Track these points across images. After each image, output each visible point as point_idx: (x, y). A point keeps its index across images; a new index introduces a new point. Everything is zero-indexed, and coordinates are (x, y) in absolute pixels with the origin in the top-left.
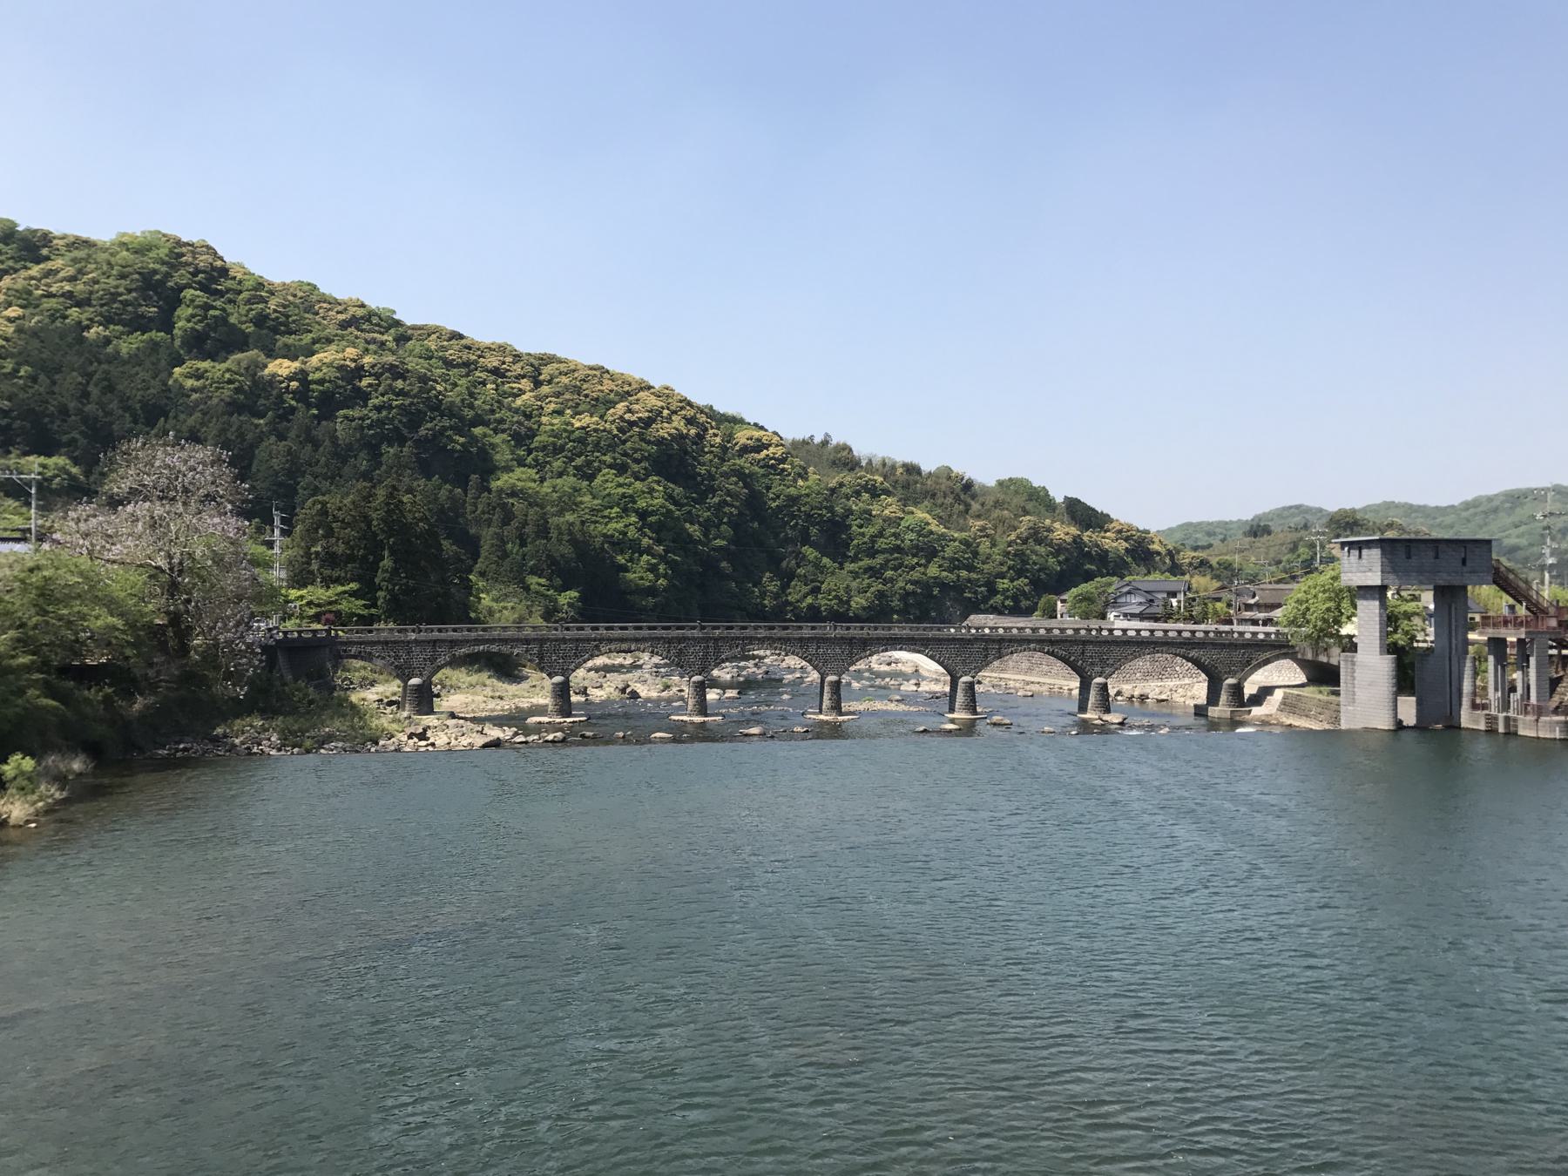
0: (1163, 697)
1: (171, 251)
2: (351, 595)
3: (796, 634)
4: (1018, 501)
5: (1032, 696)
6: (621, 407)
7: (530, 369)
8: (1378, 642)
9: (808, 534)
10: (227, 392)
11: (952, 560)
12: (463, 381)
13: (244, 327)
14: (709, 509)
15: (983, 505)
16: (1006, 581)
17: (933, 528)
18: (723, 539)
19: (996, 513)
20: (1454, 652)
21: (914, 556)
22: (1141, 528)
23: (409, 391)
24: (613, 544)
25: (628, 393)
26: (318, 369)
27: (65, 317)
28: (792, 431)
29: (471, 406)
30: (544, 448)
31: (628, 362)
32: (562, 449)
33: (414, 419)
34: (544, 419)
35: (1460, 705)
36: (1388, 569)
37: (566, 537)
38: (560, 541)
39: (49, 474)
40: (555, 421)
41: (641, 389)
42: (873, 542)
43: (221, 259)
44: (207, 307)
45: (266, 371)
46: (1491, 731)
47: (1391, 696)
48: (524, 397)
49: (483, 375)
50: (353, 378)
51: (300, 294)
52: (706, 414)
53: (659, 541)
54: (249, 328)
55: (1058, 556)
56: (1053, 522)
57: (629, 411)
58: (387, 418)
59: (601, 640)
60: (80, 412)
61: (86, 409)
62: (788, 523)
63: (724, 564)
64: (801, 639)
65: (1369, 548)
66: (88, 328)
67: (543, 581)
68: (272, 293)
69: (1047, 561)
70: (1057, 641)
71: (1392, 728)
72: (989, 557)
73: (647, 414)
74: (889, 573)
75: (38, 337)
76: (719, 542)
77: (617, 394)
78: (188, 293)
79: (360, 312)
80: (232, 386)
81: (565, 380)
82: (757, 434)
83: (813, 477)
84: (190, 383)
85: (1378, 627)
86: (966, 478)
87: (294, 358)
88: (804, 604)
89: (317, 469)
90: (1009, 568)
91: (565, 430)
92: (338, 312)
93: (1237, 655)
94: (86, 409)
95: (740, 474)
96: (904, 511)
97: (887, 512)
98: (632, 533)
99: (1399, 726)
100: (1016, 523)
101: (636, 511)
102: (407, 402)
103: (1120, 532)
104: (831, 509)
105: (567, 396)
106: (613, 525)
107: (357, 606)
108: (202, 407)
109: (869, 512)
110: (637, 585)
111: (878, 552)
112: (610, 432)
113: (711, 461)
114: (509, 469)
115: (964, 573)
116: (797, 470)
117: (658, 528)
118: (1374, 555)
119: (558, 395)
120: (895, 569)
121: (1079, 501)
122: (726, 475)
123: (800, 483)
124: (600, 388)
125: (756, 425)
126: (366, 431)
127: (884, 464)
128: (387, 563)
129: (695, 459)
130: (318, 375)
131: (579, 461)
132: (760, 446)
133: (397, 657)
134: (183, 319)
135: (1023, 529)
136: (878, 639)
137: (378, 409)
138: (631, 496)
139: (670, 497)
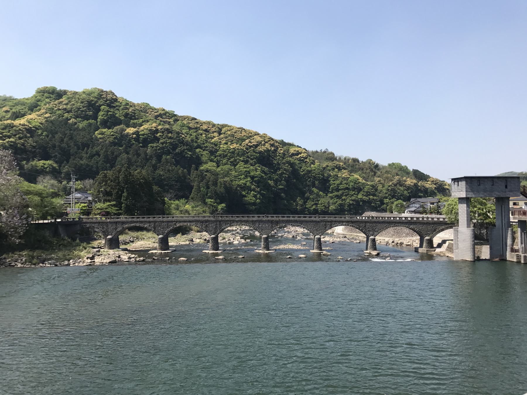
0: (409, 244)
1: (98, 94)
2: (112, 206)
3: (251, 219)
4: (394, 171)
5: (359, 243)
6: (247, 141)
7: (217, 129)
8: (466, 222)
9: (315, 184)
10: (111, 139)
11: (367, 192)
12: (195, 134)
13: (121, 118)
14: (277, 175)
15: (381, 172)
16: (387, 200)
17: (360, 181)
18: (283, 185)
19: (385, 175)
20: (504, 227)
21: (353, 191)
22: (442, 180)
23: (173, 137)
24: (241, 188)
25: (251, 136)
26: (143, 131)
27: (64, 116)
28: (311, 147)
29: (196, 142)
30: (220, 155)
31: (251, 126)
32: (226, 156)
33: (174, 146)
34: (221, 146)
35: (506, 250)
36: (469, 190)
37: (223, 186)
38: (220, 187)
39: (46, 166)
40: (225, 146)
41: (256, 135)
42: (338, 187)
43: (116, 96)
44: (108, 111)
45: (126, 132)
46: (519, 262)
47: (472, 246)
48: (215, 139)
49: (201, 132)
50: (155, 133)
51: (143, 107)
52: (278, 143)
53: (258, 187)
54: (122, 118)
55: (408, 190)
56: (407, 178)
57: (250, 142)
58: (166, 146)
59: (177, 222)
60: (59, 146)
61: (62, 145)
62: (307, 180)
63: (283, 195)
64: (252, 221)
65: (461, 181)
66: (70, 119)
67: (212, 200)
68: (131, 106)
69: (403, 192)
70: (355, 222)
71: (472, 260)
72: (381, 191)
73: (256, 143)
74: (343, 198)
75: (52, 123)
76: (281, 187)
77: (247, 136)
78: (102, 107)
79: (163, 112)
80: (113, 137)
81: (229, 133)
82: (297, 149)
83: (317, 164)
84: (99, 136)
85: (466, 215)
86: (376, 163)
87: (135, 128)
88: (312, 208)
89: (138, 164)
90: (389, 195)
91: (228, 149)
92: (155, 112)
93: (430, 227)
94: (62, 145)
95: (289, 163)
96: (350, 175)
97: (343, 175)
98: (248, 184)
99: (477, 259)
100: (393, 179)
101: (250, 176)
102: (173, 140)
103: (433, 181)
104: (323, 175)
105: (229, 138)
106: (242, 181)
107: (114, 210)
108: (102, 144)
109: (337, 176)
110: (249, 202)
111: (340, 190)
112: (243, 150)
113: (279, 159)
114: (206, 163)
115: (371, 197)
116: (311, 161)
117: (258, 182)
118: (463, 184)
119: (226, 138)
120: (346, 196)
121: (418, 171)
122: (284, 164)
123: (312, 166)
124: (241, 135)
125: (298, 146)
126: (158, 151)
127: (345, 159)
128: (125, 194)
129: (273, 158)
130: (142, 133)
131: (232, 160)
132: (298, 153)
133: (103, 228)
134: (101, 116)
135: (395, 181)
136: (282, 221)
137: (162, 143)
138: (248, 171)
139: (263, 172)
